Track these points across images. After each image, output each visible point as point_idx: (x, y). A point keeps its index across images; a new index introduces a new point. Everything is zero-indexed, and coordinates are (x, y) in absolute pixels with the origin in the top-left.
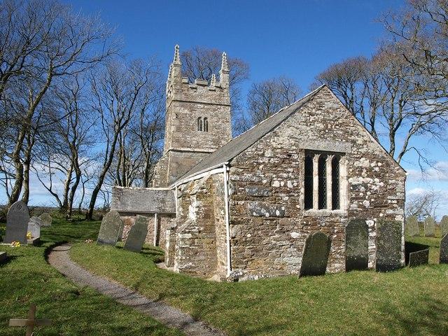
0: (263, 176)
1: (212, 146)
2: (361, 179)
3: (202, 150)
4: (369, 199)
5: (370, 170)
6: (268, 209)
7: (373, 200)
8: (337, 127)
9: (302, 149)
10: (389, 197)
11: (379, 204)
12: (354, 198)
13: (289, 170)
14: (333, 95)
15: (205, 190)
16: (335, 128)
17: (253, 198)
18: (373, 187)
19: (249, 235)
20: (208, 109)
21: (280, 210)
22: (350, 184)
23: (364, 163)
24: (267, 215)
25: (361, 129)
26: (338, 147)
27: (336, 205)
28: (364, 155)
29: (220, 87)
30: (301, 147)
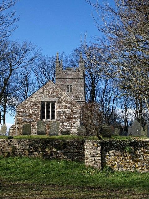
2: (62, 109)
4: (65, 116)
6: (28, 119)
7: (66, 116)
10: (74, 115)
12: (59, 116)
17: (24, 116)
18: (67, 112)
19: (22, 127)
20: (72, 81)
21: (32, 120)
22: (57, 111)
23: (64, 104)
24: (28, 121)
25: (63, 93)
26: (53, 99)
27: (53, 118)
28: (63, 101)
29: (78, 70)
30: (40, 100)
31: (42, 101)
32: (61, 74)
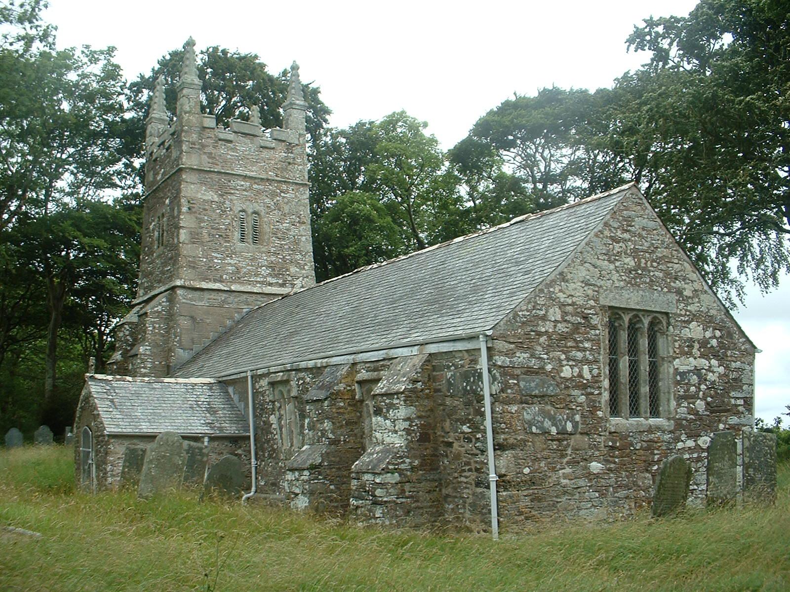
0: (545, 356)
1: (269, 279)
3: (249, 288)
5: (704, 343)
6: (552, 419)
8: (655, 264)
9: (604, 306)
11: (719, 408)
13: (587, 345)
14: (647, 205)
15: (419, 385)
16: (652, 266)
19: (526, 471)
20: (259, 192)
28: (694, 317)
30: (603, 302)
31: (611, 308)
32: (210, 149)
